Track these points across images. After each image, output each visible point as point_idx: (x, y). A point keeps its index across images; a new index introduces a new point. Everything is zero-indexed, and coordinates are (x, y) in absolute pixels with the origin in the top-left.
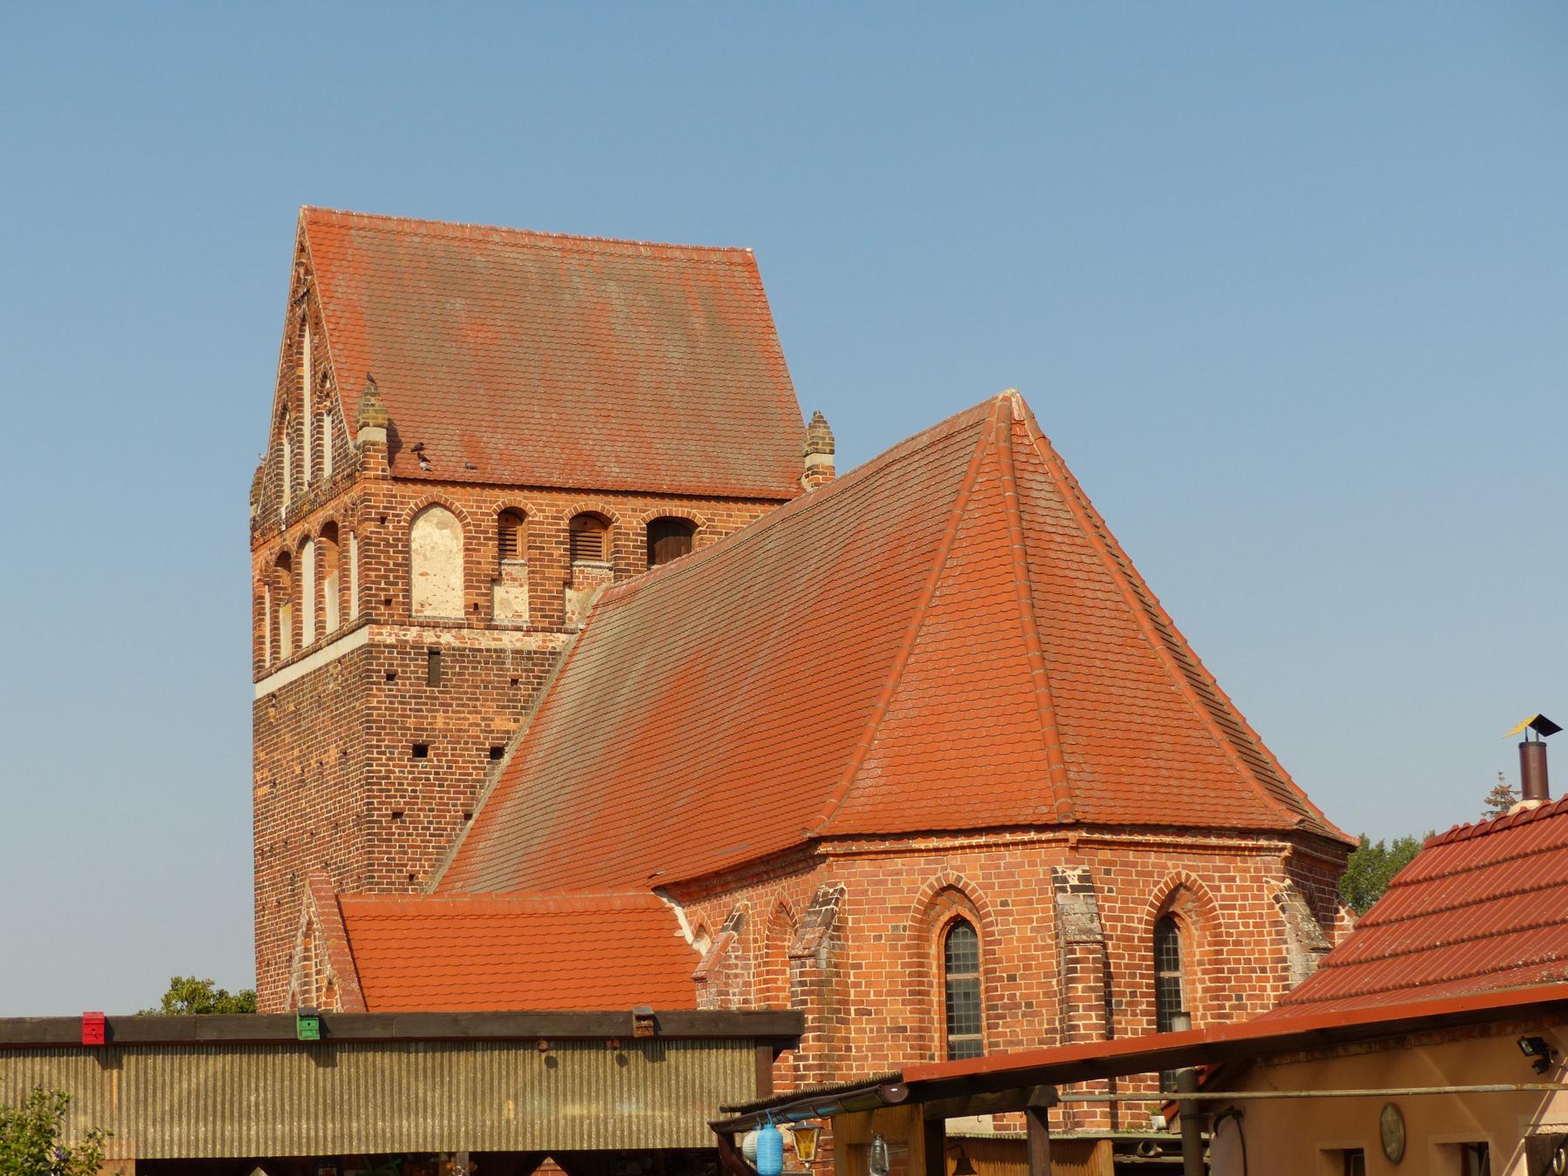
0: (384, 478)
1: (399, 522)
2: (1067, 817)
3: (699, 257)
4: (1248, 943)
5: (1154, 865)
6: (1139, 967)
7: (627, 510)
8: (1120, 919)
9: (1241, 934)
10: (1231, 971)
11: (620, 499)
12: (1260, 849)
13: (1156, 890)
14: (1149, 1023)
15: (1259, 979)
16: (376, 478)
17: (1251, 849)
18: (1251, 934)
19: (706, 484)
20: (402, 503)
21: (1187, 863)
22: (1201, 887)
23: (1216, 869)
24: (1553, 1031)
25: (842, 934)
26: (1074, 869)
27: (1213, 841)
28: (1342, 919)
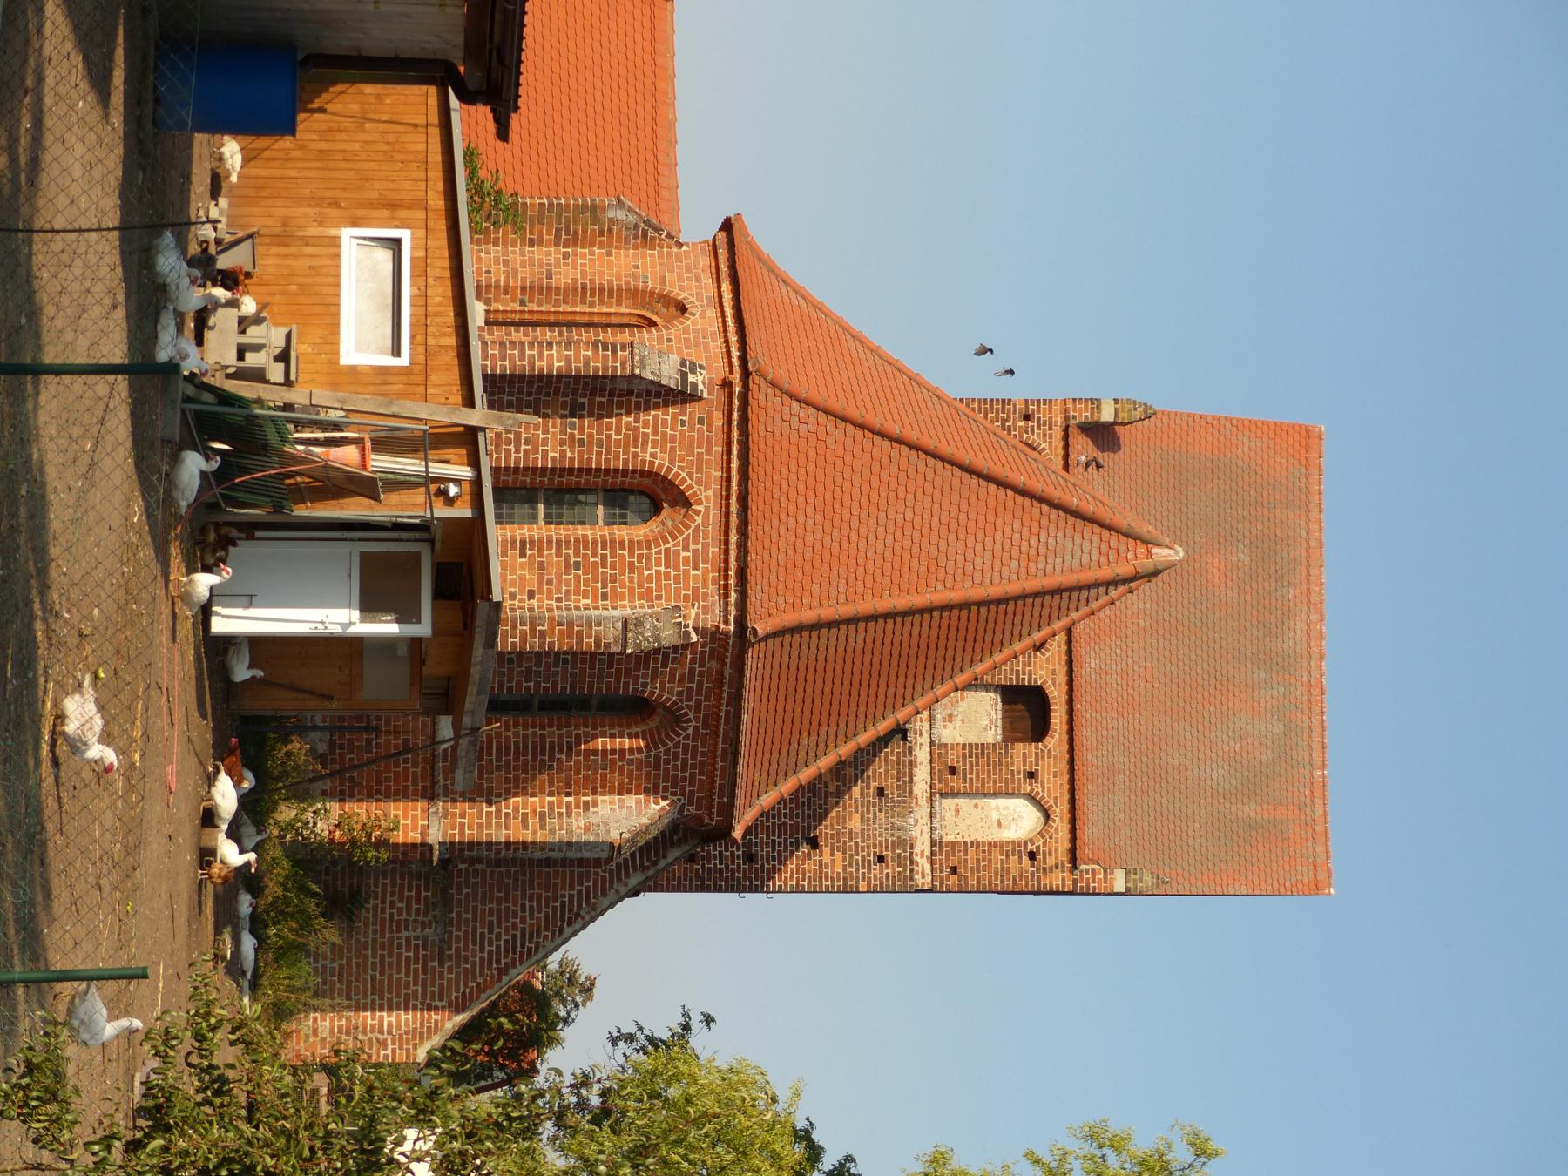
0: (1067, 418)
1: (1027, 432)
2: (754, 365)
3: (1317, 832)
4: (631, 581)
5: (708, 475)
6: (608, 452)
7: (1054, 665)
8: (655, 433)
9: (641, 574)
10: (604, 557)
11: (1064, 658)
12: (726, 596)
13: (684, 475)
14: (553, 459)
15: (595, 590)
16: (1066, 410)
17: (726, 586)
18: (641, 586)
19: (1085, 756)
20: (1045, 435)
21: (711, 513)
22: (687, 527)
23: (705, 546)
24: (540, 1081)
25: (639, 241)
26: (704, 383)
27: (733, 538)
28: (656, 803)
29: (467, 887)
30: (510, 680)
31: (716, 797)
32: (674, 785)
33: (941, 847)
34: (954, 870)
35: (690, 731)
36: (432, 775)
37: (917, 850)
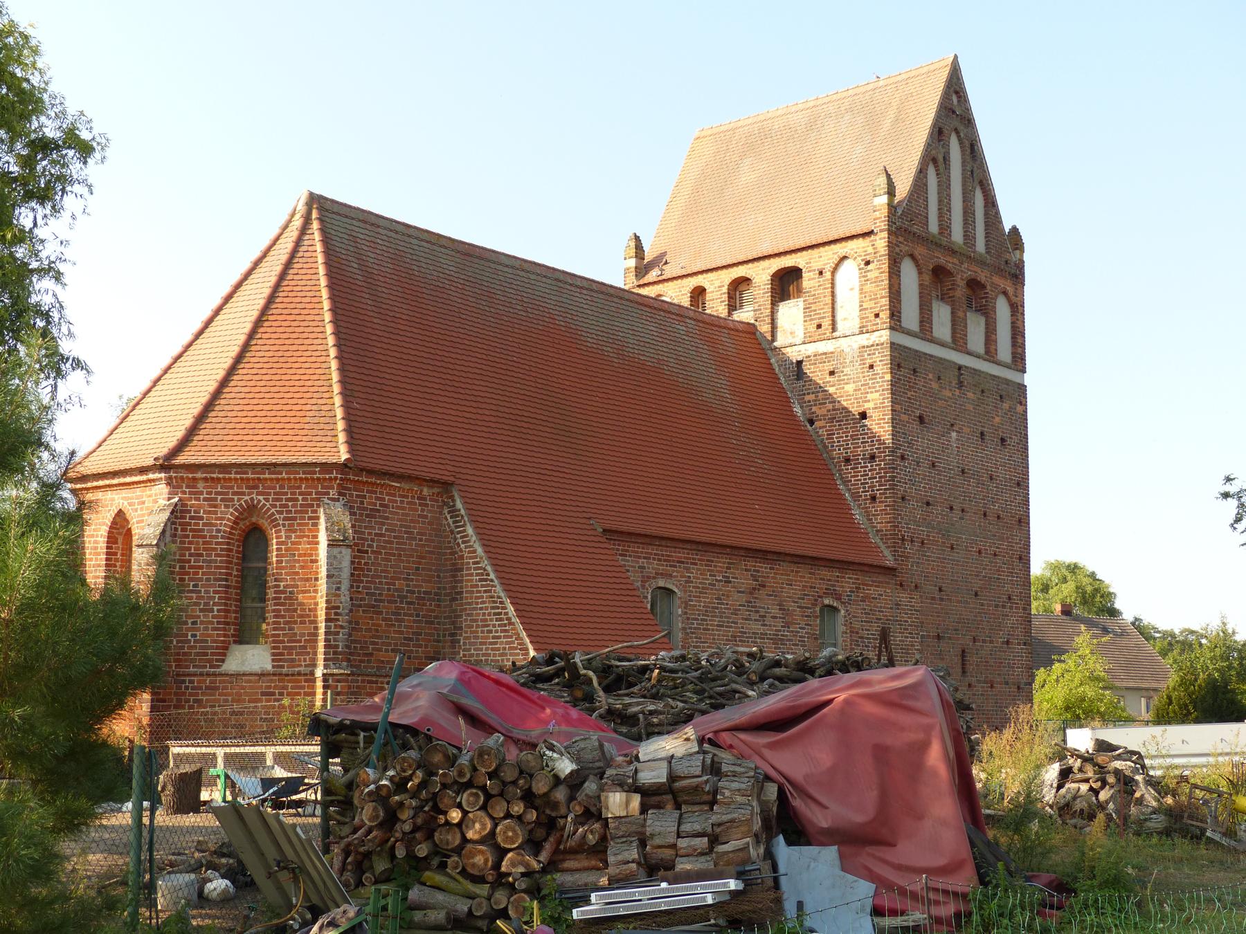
11: (756, 264)
29: (373, 649)
30: (212, 623)
31: (315, 476)
32: (312, 506)
33: (863, 327)
34: (877, 316)
35: (261, 498)
36: (293, 675)
37: (866, 343)
